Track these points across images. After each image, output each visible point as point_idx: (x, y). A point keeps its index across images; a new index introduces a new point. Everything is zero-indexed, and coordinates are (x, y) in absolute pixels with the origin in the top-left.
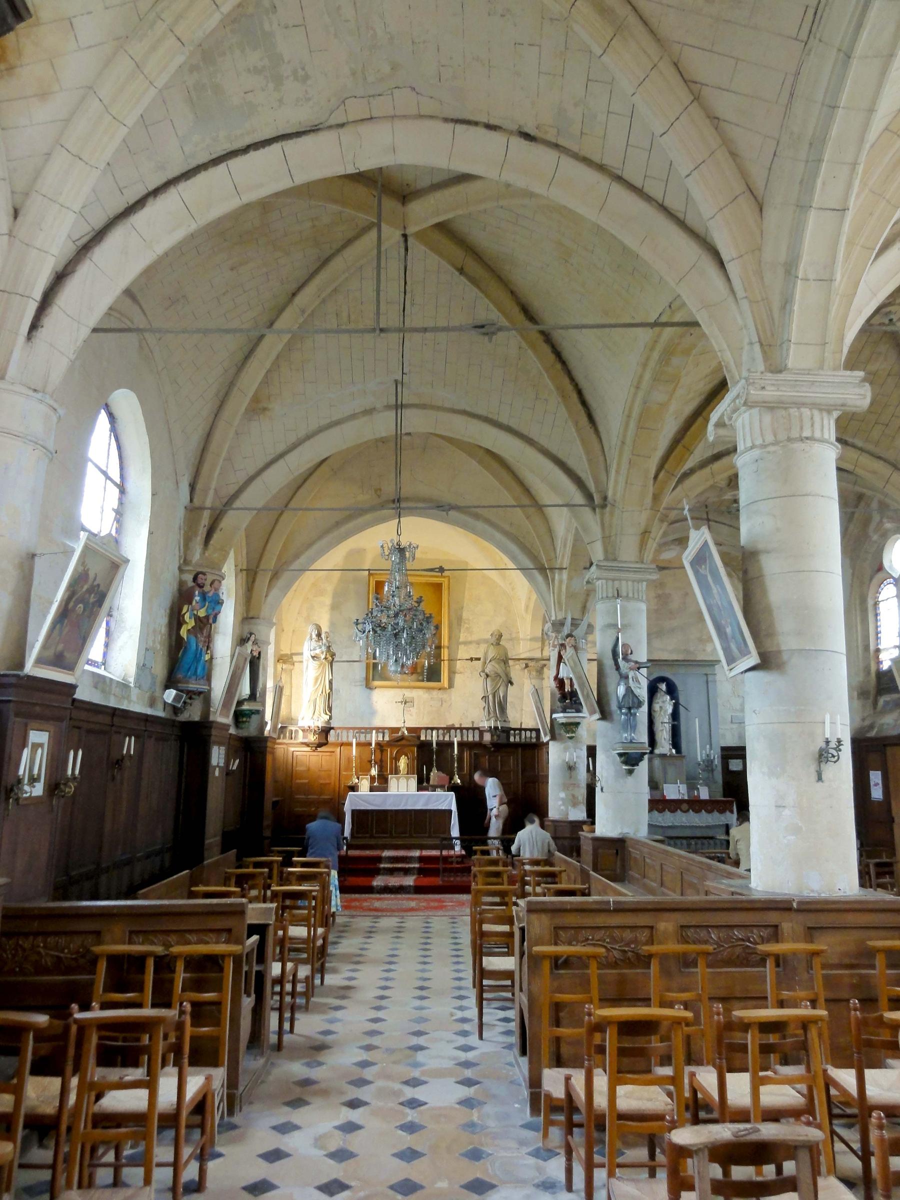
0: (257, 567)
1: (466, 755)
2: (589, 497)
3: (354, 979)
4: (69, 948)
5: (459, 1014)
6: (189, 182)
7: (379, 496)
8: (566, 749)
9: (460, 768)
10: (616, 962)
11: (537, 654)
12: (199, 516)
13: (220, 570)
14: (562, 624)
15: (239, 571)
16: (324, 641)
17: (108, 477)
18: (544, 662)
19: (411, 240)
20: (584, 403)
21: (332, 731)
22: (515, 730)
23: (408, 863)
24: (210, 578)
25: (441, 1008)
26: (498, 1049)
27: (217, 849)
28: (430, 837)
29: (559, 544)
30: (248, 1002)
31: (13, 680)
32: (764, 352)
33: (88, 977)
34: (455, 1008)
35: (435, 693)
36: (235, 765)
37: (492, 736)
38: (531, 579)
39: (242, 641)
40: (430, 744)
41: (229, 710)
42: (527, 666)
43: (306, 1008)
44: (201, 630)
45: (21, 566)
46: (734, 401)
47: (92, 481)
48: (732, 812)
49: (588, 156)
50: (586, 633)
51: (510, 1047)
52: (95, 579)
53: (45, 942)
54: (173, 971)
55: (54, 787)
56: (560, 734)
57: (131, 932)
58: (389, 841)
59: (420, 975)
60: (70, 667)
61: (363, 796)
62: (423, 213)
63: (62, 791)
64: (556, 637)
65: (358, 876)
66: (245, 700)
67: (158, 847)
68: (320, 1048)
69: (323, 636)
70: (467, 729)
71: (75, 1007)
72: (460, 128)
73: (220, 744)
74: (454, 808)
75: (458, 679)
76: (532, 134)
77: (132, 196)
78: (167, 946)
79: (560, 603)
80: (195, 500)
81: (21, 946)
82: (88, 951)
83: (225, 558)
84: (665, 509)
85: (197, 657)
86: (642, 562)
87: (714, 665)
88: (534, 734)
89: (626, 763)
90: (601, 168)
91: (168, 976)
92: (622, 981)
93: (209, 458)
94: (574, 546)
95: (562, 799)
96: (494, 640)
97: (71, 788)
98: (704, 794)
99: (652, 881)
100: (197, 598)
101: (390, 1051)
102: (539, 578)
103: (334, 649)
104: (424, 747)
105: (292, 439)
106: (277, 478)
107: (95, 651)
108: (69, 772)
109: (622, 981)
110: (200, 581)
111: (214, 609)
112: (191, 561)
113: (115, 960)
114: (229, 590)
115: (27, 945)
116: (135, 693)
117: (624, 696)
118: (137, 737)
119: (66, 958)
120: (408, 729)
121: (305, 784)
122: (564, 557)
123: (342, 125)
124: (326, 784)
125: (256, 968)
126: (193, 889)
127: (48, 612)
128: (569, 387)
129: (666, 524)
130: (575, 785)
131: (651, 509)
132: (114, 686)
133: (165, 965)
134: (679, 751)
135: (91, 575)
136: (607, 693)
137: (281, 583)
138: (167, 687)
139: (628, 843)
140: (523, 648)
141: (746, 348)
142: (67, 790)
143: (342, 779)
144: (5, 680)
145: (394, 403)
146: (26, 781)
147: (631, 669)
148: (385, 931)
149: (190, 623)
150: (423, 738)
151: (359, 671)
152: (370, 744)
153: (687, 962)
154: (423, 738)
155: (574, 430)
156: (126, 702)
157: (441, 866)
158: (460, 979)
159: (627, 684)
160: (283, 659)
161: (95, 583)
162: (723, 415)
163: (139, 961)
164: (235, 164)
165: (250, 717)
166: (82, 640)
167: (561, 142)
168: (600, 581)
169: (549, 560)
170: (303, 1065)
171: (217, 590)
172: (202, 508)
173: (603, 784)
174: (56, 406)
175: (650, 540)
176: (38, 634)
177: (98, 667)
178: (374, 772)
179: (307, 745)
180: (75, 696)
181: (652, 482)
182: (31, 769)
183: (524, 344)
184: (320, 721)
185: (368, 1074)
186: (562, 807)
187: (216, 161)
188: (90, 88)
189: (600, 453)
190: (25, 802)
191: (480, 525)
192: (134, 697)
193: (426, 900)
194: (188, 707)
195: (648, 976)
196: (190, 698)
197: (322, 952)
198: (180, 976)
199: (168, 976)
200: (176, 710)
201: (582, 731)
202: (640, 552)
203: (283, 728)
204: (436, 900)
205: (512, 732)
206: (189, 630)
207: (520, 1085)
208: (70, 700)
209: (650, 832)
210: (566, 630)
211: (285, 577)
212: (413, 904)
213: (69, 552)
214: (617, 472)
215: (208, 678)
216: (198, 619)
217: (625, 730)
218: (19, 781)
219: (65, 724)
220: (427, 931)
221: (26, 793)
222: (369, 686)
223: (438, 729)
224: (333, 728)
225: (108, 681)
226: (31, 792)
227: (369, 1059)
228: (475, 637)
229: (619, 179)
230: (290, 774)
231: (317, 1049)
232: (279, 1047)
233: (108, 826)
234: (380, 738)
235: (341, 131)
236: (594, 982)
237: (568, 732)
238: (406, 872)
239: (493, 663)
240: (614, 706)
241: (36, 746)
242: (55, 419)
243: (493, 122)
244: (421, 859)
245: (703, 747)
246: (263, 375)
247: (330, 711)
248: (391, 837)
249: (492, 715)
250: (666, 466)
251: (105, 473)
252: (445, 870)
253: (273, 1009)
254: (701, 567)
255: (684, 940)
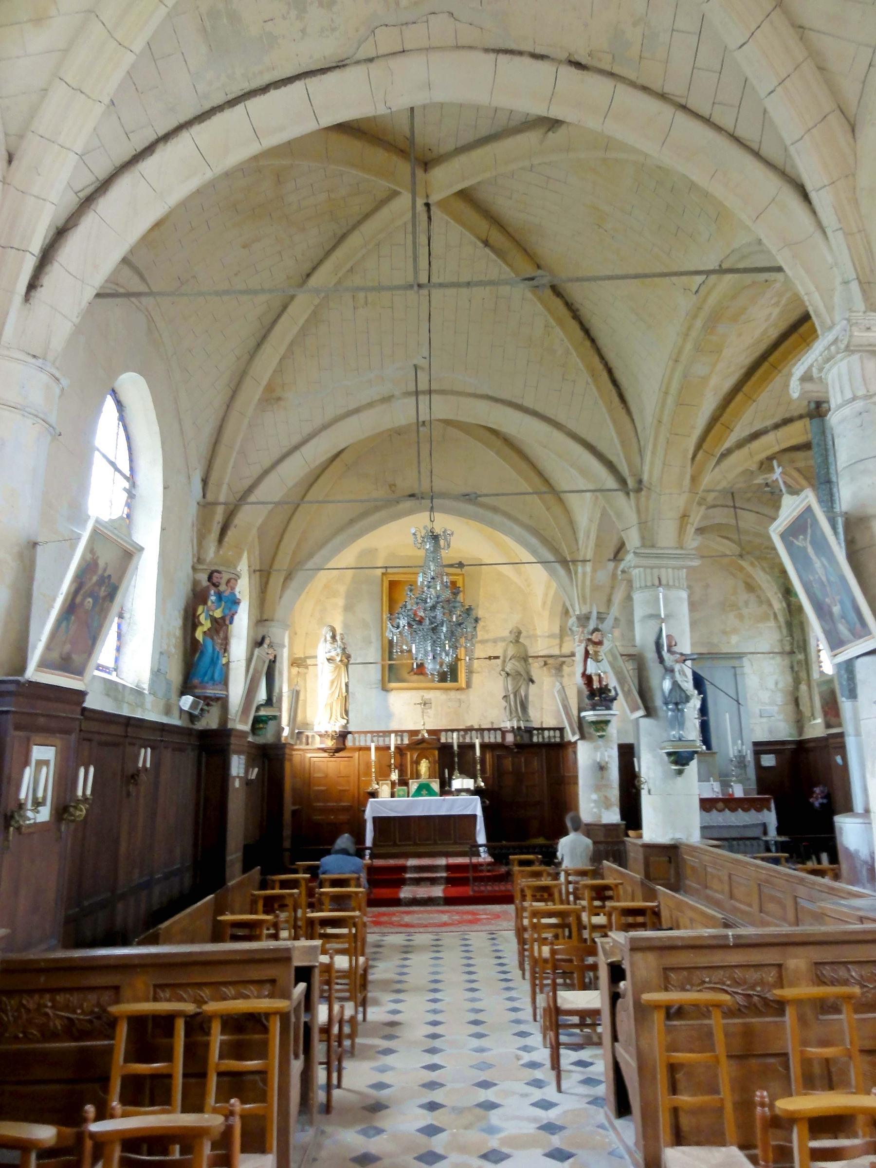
0: (271, 567)
1: (488, 756)
2: (623, 481)
3: (398, 1012)
4: (81, 1007)
5: (527, 1057)
6: (203, 125)
7: (393, 492)
8: (596, 749)
9: (483, 771)
10: (739, 1010)
11: (556, 651)
12: (212, 512)
13: (235, 568)
14: (587, 618)
15: (253, 572)
16: (339, 642)
17: (117, 469)
18: (563, 659)
19: (433, 208)
20: (615, 382)
21: (349, 736)
22: (537, 729)
23: (436, 872)
24: (225, 577)
25: (503, 1047)
26: (582, 1104)
27: (238, 866)
28: (455, 843)
29: (581, 535)
30: (297, 1066)
31: (12, 688)
32: (864, 292)
33: (106, 1042)
34: (519, 1049)
35: (453, 694)
36: (254, 773)
37: (515, 736)
38: (552, 573)
39: (259, 643)
40: (450, 746)
41: (248, 717)
42: (546, 664)
43: (352, 1053)
44: (217, 632)
45: (21, 556)
46: (828, 348)
47: (100, 471)
48: (769, 809)
49: (646, 84)
50: (613, 627)
51: (595, 1101)
52: (105, 570)
53: (53, 1000)
54: (208, 1033)
55: (61, 811)
56: (590, 733)
57: (156, 986)
58: (412, 849)
59: (471, 1005)
60: (79, 672)
61: (387, 801)
62: (445, 180)
63: (72, 815)
64: (583, 632)
65: (385, 887)
66: (262, 705)
67: (178, 866)
68: (376, 1108)
69: (338, 638)
70: (489, 730)
71: (90, 1109)
72: (503, 58)
73: (239, 753)
74: (479, 812)
75: (476, 678)
76: (583, 62)
77: (139, 142)
78: (200, 1002)
79: (584, 597)
80: (208, 495)
81: (24, 1006)
82: (105, 1011)
83: (239, 557)
84: (704, 491)
85: (214, 662)
86: (682, 548)
87: (740, 658)
88: (558, 733)
89: (676, 763)
90: (663, 96)
91: (201, 1039)
92: (748, 1033)
93: (222, 449)
94: (598, 537)
95: (595, 801)
96: (512, 638)
97: (81, 810)
98: (738, 792)
99: (716, 891)
100: (213, 598)
101: (458, 1111)
102: (562, 572)
103: (349, 650)
104: (446, 749)
105: (307, 429)
106: (294, 470)
107: (105, 654)
108: (80, 793)
109: (748, 1033)
110: (215, 580)
111: (230, 609)
112: (205, 560)
113: (138, 1022)
114: (244, 588)
115: (31, 1006)
116: (149, 700)
117: (671, 691)
118: (153, 749)
119: (78, 1019)
120: (429, 731)
121: (322, 791)
122: (587, 548)
123: (371, 60)
124: (345, 791)
125: (303, 1019)
126: (219, 918)
127: (52, 607)
128: (600, 367)
129: (703, 508)
130: (608, 786)
131: (690, 492)
132: (127, 692)
133: (197, 1025)
134: (709, 747)
135: (101, 563)
136: (650, 689)
137: (294, 584)
138: (183, 693)
139: (683, 850)
140: (541, 646)
141: (839, 288)
142: (78, 813)
143: (362, 785)
144: (4, 688)
145: (414, 389)
146: (29, 805)
147: (677, 661)
148: (422, 948)
149: (206, 624)
150: (443, 740)
151: (374, 673)
152: (389, 748)
153: (826, 1007)
154: (443, 740)
155: (604, 410)
156: (140, 710)
157: (470, 875)
158: (515, 1010)
159: (673, 677)
160: (297, 662)
161: (106, 575)
162: (812, 366)
163: (166, 1022)
164: (254, 104)
165: (267, 723)
166: (90, 639)
167: (616, 70)
168: (637, 570)
169: (571, 553)
170: (358, 1132)
171: (233, 589)
172: (215, 504)
173: (651, 786)
174: (58, 375)
175: (689, 526)
176: (41, 632)
177: (109, 673)
178: (395, 776)
179: (324, 750)
180: (86, 705)
181: (689, 462)
182: (35, 790)
183: (553, 323)
184: (337, 726)
185: (438, 1143)
186: (595, 810)
187: (232, 103)
188: (90, 11)
189: (632, 434)
190: (30, 830)
191: (498, 518)
192: (148, 706)
193: (458, 913)
194: (206, 714)
195: (781, 1026)
196: (208, 705)
197: (364, 983)
198: (217, 1038)
199: (201, 1039)
200: (192, 718)
201: (612, 729)
202: (680, 536)
203: (300, 733)
204: (468, 913)
205: (535, 732)
206: (205, 633)
207: (622, 1157)
208: (79, 710)
209: (703, 837)
210: (592, 625)
211: (300, 576)
212: (445, 918)
213: (74, 540)
214: (653, 453)
215: (225, 682)
216: (214, 620)
217: (673, 728)
218: (21, 806)
219: (73, 737)
220: (466, 948)
221: (29, 819)
222: (385, 689)
223: (458, 730)
224: (350, 733)
225: (120, 688)
226: (35, 819)
227: (435, 1123)
228: (491, 636)
229: (684, 108)
230: (307, 780)
231: (373, 1109)
232: (327, 1108)
233: (123, 848)
234: (399, 742)
235: (372, 66)
236: (719, 1038)
237: (597, 731)
238: (433, 881)
239: (513, 661)
240: (658, 702)
241: (40, 763)
242: (57, 391)
243: (539, 50)
244: (448, 868)
245: (734, 743)
246: (278, 361)
247: (347, 714)
248: (415, 844)
249: (514, 714)
250: (705, 446)
251: (113, 464)
252: (476, 879)
253: (321, 1063)
254: (797, 538)
255: (821, 981)
